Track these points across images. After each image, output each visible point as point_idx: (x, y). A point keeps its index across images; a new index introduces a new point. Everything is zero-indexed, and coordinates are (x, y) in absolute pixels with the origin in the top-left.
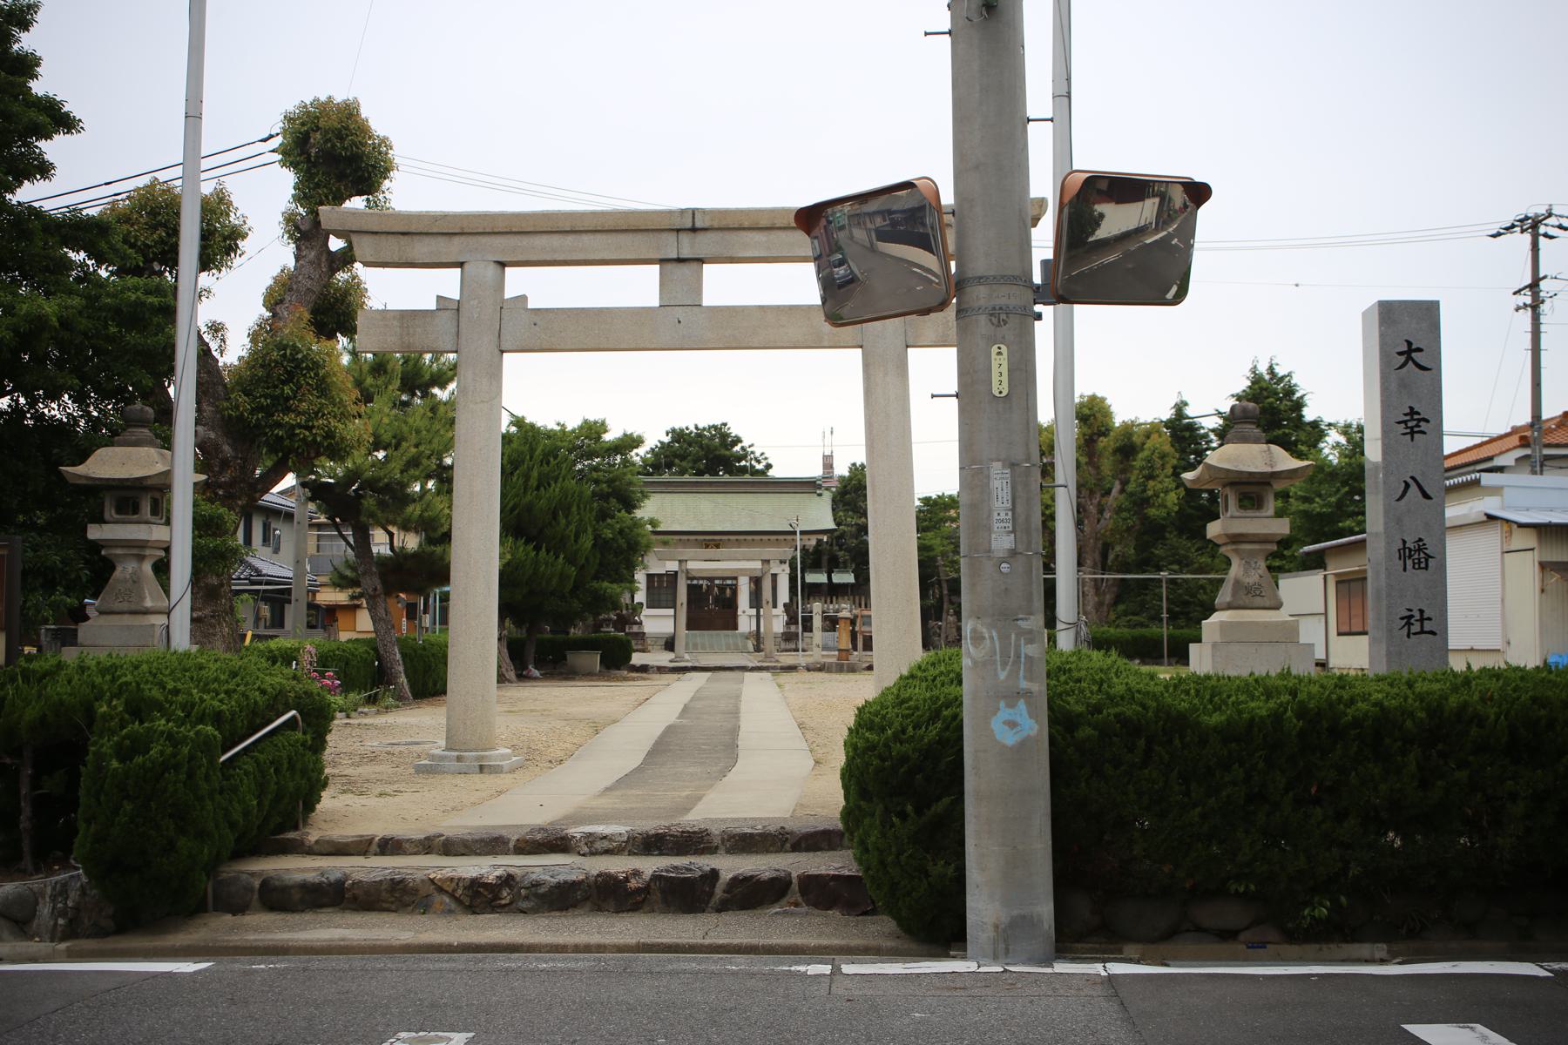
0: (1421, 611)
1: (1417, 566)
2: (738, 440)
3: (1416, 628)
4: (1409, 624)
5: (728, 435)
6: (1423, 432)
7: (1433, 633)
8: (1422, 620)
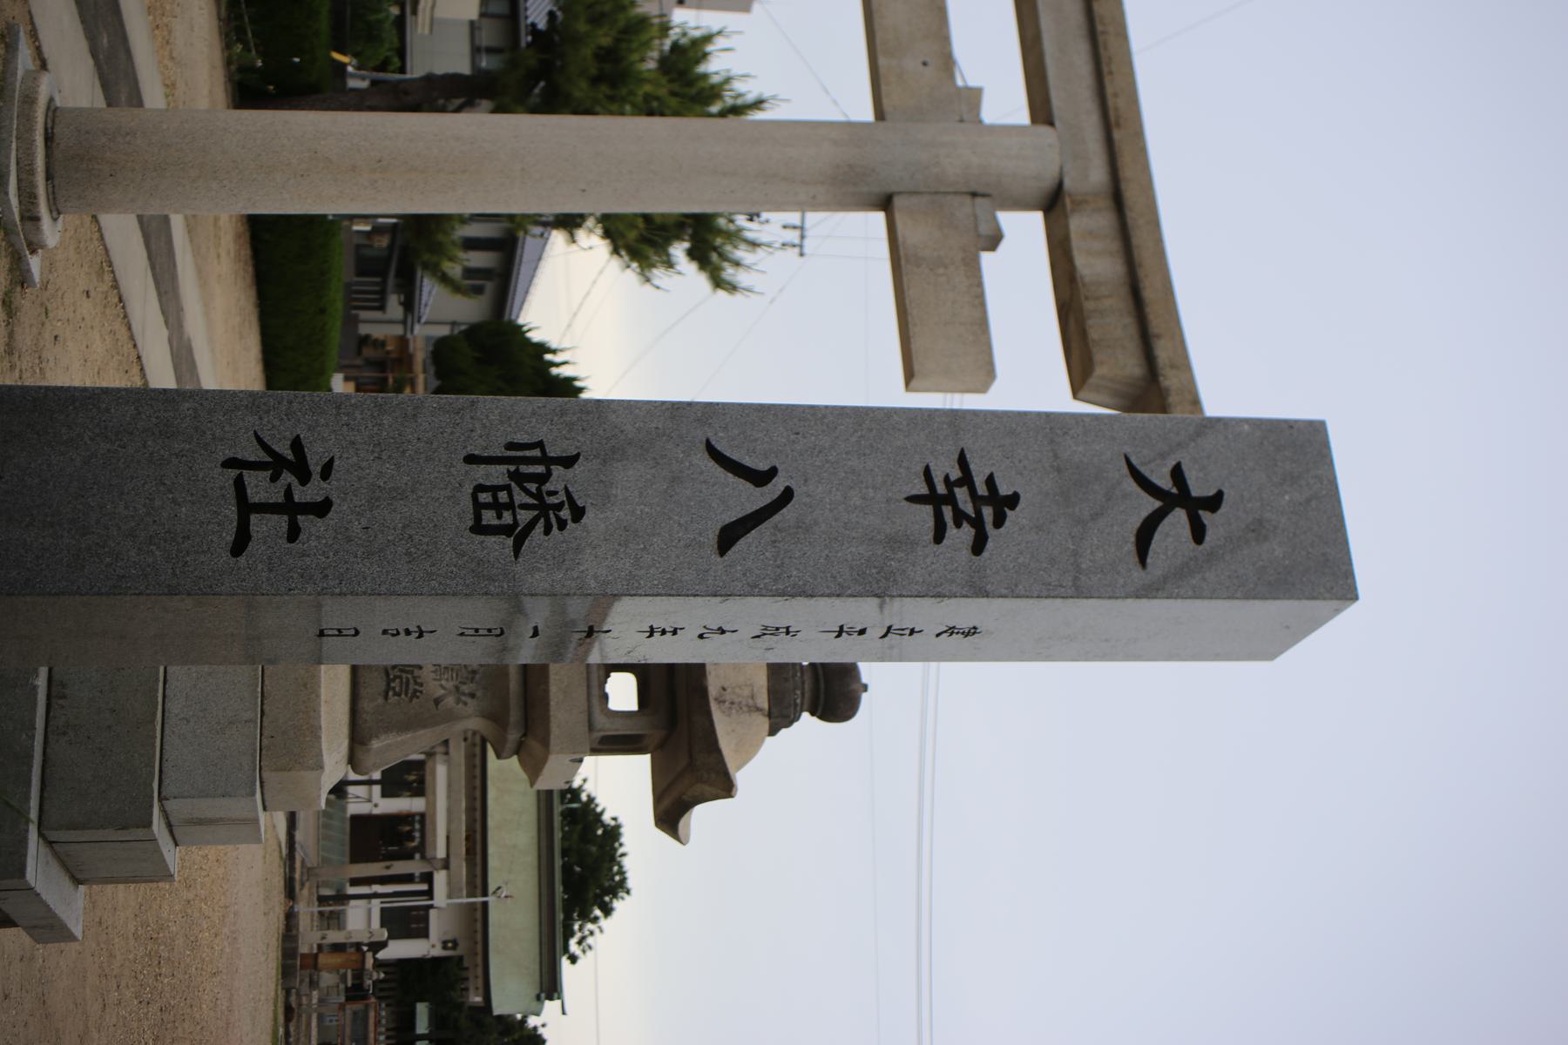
0: (322, 508)
1: (485, 500)
2: (607, 911)
3: (260, 487)
4: (276, 465)
5: (615, 896)
6: (939, 536)
7: (241, 543)
8: (289, 507)
